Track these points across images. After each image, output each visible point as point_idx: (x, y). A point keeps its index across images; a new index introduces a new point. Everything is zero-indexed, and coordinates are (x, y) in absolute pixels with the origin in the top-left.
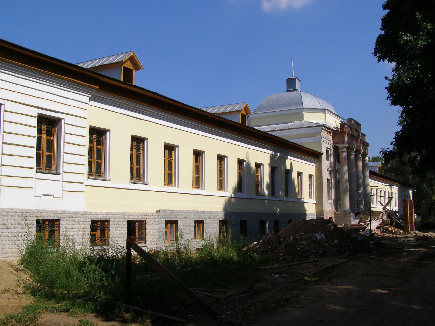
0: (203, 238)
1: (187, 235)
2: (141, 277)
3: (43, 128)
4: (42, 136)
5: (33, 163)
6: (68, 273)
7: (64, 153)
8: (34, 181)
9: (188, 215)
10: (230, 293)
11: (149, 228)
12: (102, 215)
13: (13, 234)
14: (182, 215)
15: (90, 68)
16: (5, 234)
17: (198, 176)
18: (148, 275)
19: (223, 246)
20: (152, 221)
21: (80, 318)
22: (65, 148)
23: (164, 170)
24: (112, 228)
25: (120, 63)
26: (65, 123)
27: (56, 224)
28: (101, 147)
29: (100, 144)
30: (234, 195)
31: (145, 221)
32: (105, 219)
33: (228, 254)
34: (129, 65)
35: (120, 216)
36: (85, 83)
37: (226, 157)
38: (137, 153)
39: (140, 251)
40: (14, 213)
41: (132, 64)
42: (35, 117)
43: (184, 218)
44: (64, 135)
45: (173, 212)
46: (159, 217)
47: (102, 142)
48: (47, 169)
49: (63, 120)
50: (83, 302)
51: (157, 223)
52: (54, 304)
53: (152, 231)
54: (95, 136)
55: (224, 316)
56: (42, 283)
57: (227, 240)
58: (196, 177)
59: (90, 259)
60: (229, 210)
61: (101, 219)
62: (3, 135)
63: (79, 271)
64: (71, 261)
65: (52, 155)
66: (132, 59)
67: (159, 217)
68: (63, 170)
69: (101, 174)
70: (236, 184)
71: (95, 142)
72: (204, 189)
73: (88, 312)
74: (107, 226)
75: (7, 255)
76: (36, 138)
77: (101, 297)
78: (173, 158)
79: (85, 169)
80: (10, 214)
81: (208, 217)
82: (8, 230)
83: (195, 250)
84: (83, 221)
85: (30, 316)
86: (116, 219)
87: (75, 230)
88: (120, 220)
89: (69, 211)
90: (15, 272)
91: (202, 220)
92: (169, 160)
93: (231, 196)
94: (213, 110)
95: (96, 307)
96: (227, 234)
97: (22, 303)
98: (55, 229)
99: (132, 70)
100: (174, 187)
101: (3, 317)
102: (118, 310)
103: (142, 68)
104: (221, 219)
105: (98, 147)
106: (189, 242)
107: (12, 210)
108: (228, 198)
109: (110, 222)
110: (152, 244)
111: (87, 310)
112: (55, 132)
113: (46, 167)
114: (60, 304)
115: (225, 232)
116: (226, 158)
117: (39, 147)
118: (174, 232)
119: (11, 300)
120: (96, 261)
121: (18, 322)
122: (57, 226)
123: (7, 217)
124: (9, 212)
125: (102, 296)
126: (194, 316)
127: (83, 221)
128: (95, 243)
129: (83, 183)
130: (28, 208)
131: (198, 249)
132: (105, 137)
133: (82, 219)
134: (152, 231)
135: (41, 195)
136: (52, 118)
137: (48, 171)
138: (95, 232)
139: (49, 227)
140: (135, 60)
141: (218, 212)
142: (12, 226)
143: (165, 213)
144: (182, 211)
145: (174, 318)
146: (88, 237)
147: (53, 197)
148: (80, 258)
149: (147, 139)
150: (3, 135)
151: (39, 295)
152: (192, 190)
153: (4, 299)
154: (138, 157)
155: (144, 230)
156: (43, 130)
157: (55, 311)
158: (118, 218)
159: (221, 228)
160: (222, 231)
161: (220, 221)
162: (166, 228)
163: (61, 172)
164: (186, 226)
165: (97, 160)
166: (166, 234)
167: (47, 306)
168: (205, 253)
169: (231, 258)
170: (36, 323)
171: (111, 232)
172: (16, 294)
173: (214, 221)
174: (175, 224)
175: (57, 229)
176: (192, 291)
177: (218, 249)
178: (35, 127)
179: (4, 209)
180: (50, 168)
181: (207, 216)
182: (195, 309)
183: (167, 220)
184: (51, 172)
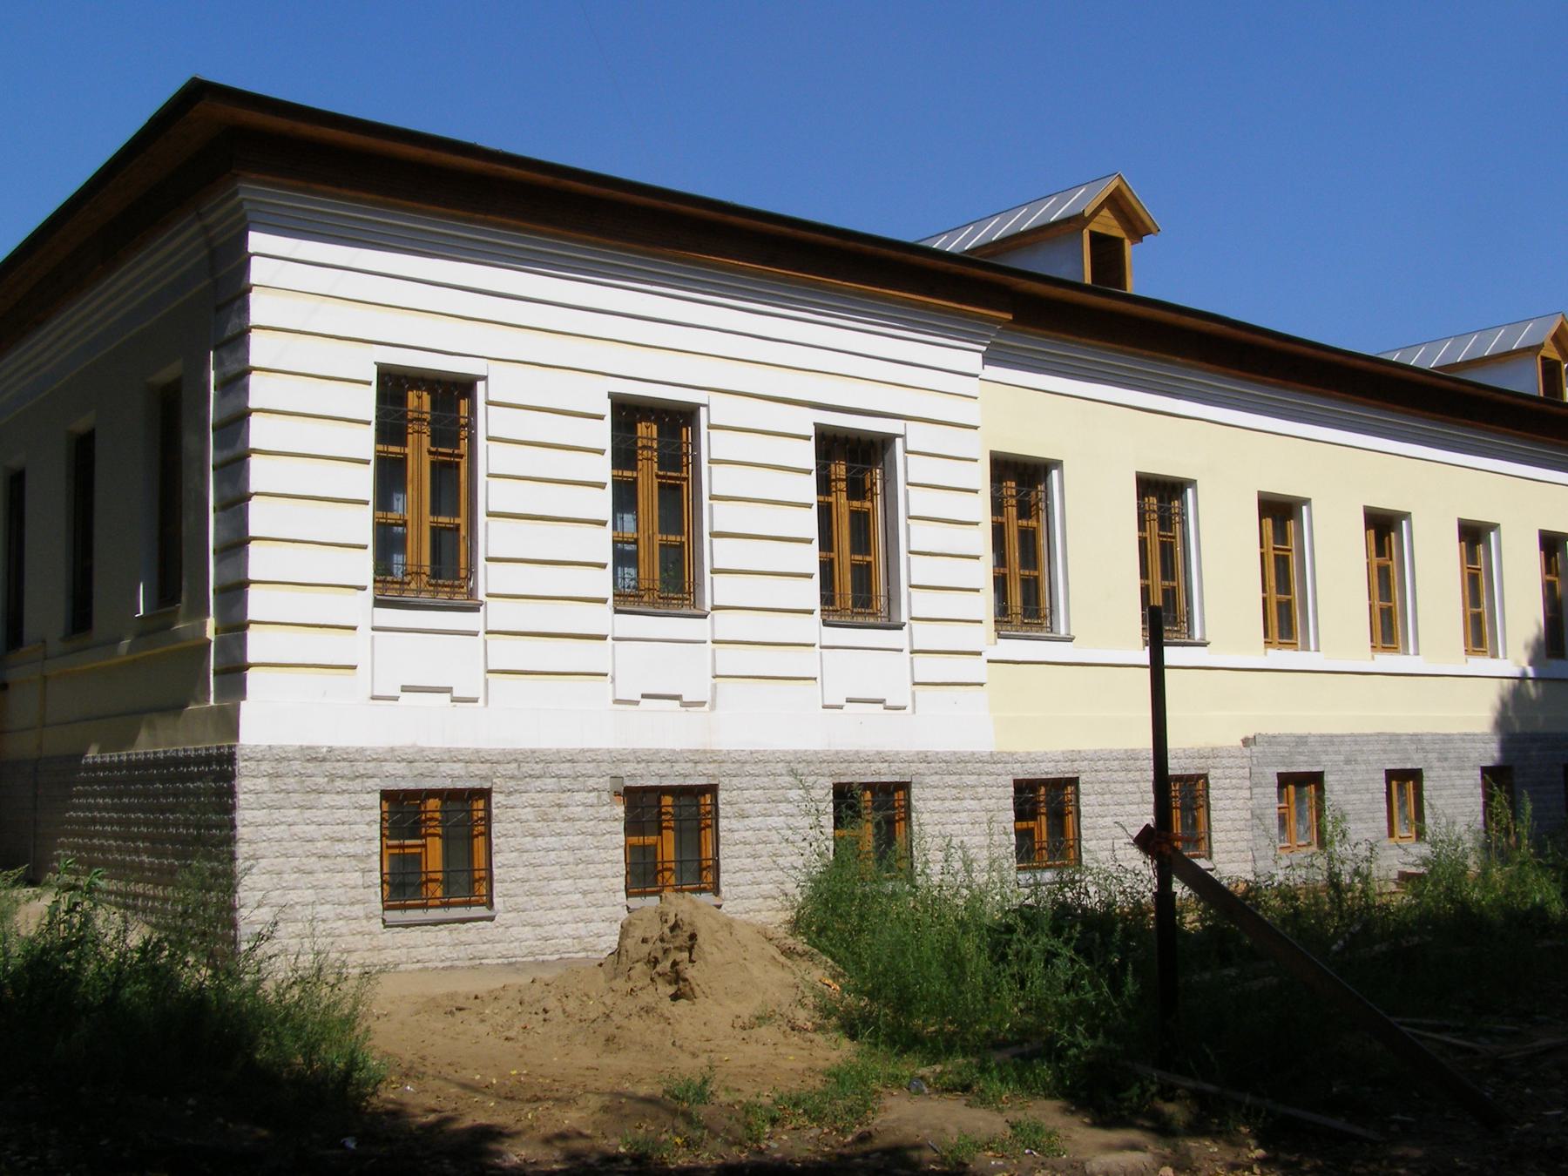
0: (1420, 835)
1: (1360, 825)
2: (1207, 976)
3: (836, 474)
4: (832, 499)
5: (809, 593)
6: (953, 962)
7: (911, 552)
8: (610, 648)
9: (1362, 752)
10: (1544, 1042)
11: (1221, 804)
12: (1053, 763)
13: (761, 834)
14: (1338, 753)
15: (973, 251)
16: (736, 836)
17: (1390, 604)
18: (1233, 972)
19: (1506, 862)
20: (1230, 778)
21: (1011, 1115)
22: (914, 536)
23: (1264, 590)
24: (1088, 808)
25: (1074, 223)
26: (907, 452)
27: (899, 800)
28: (1032, 523)
29: (1030, 512)
30: (1536, 670)
31: (1205, 777)
32: (1061, 776)
33: (1525, 895)
34: (1108, 224)
35: (1113, 763)
36: (964, 307)
37: (1494, 527)
38: (1162, 536)
39: (1205, 885)
40: (761, 765)
41: (1117, 218)
42: (808, 438)
43: (1348, 762)
44: (907, 492)
45: (1305, 743)
46: (1255, 762)
47: (1037, 504)
48: (858, 613)
49: (899, 441)
50: (1015, 1063)
51: (1247, 783)
52: (918, 1068)
53: (1230, 814)
54: (1010, 487)
55: (1529, 1125)
56: (873, 995)
57: (1518, 840)
58: (1381, 609)
59: (1027, 915)
60: (1517, 728)
61: (1049, 776)
62: (711, 507)
63: (990, 958)
64: (961, 923)
65: (869, 563)
66: (1117, 203)
67: (1255, 762)
68: (910, 612)
69: (1038, 618)
70: (1540, 628)
71: (1012, 506)
72: (1417, 654)
73: (1034, 1096)
74: (1071, 801)
75: (747, 904)
76: (815, 507)
77: (1078, 1046)
78: (1293, 544)
79: (984, 604)
80: (748, 768)
81: (1435, 755)
82: (747, 822)
83: (1394, 881)
84: (986, 786)
85: (848, 1103)
86: (1101, 776)
87: (964, 816)
88: (1115, 776)
89: (937, 753)
90: (782, 959)
91: (1415, 767)
92: (1277, 552)
93: (1524, 673)
94: (1427, 357)
95: (1060, 1078)
96: (1514, 817)
97: (817, 1059)
98: (894, 815)
99: (1118, 243)
100: (1302, 650)
101: (768, 1101)
102: (1135, 1090)
103: (1154, 230)
104: (1489, 763)
105: (1024, 523)
106: (1372, 849)
107: (755, 755)
108: (1511, 680)
109: (1081, 786)
110: (1233, 862)
111: (1030, 1088)
112: (875, 484)
113: (854, 605)
114: (938, 1068)
115: (1509, 812)
116: (1492, 534)
117: (826, 540)
118: (1311, 815)
119: (782, 1050)
120: (1046, 924)
121: (814, 1120)
122: (900, 806)
123: (314, 810)
124: (746, 762)
125: (1084, 1043)
126: (1413, 1120)
127: (986, 786)
128: (1034, 860)
129: (979, 654)
130: (803, 748)
131: (1404, 877)
132: (1046, 488)
133: (984, 779)
134: (1230, 814)
135: (843, 702)
136: (838, 435)
137: (860, 620)
138: (1031, 824)
139: (876, 809)
140: (1129, 204)
141: (1475, 735)
142: (757, 809)
143: (1275, 748)
144: (1337, 736)
145: (1340, 1123)
146: (1008, 842)
147: (881, 706)
148: (992, 913)
149: (1192, 483)
150: (711, 507)
151: (870, 1036)
152: (1370, 657)
153: (760, 1046)
154: (1167, 551)
155: (1202, 811)
156: (834, 480)
157: (926, 1091)
158: (1108, 770)
159: (1488, 798)
160: (1497, 808)
161: (1484, 770)
162: (1280, 801)
163: (904, 618)
164: (1355, 792)
165: (1022, 572)
166: (1283, 821)
167: (898, 1073)
168: (1436, 888)
169: (1540, 910)
170: (869, 1124)
171: (1084, 822)
172: (793, 1029)
173: (1461, 769)
174: (1313, 786)
175: (903, 815)
176: (1404, 1029)
177: (1485, 873)
178: (809, 472)
179: (729, 752)
180: (868, 607)
181: (1433, 751)
182: (1416, 1095)
183: (1284, 771)
184: (871, 620)
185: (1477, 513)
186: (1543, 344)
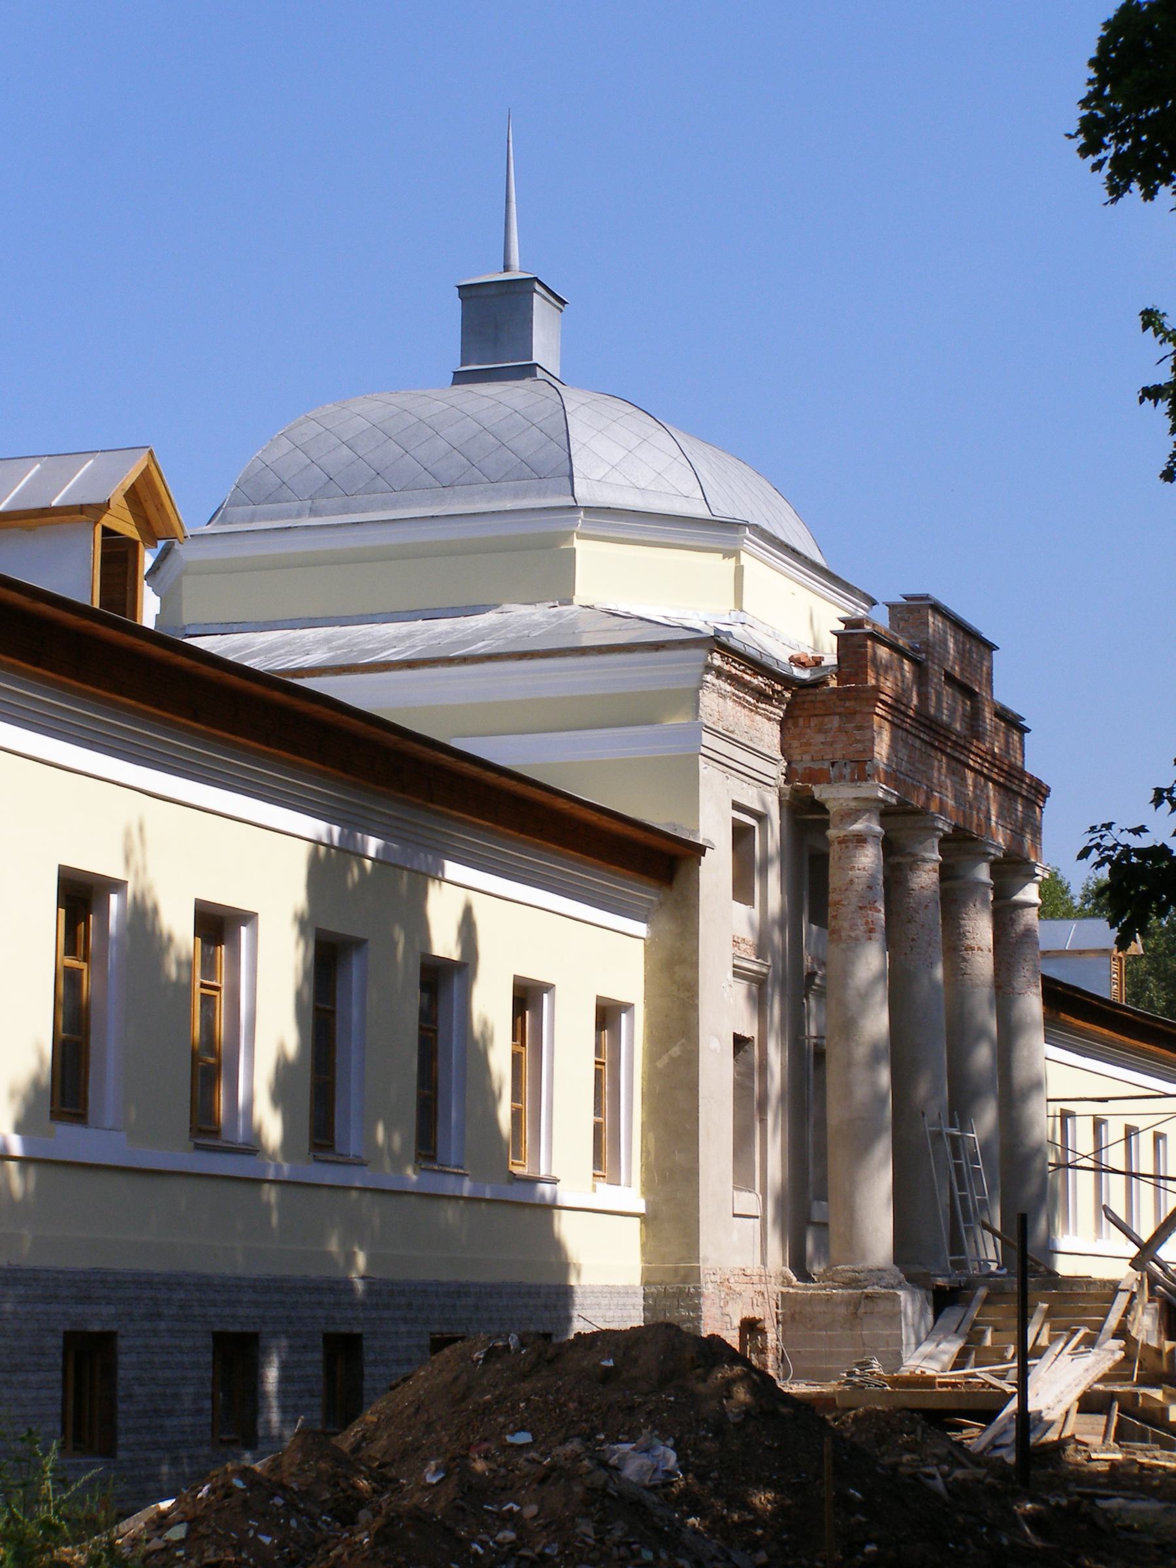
30: (26, 1144)
92: (205, 991)
185: (535, 973)
186: (107, 505)
